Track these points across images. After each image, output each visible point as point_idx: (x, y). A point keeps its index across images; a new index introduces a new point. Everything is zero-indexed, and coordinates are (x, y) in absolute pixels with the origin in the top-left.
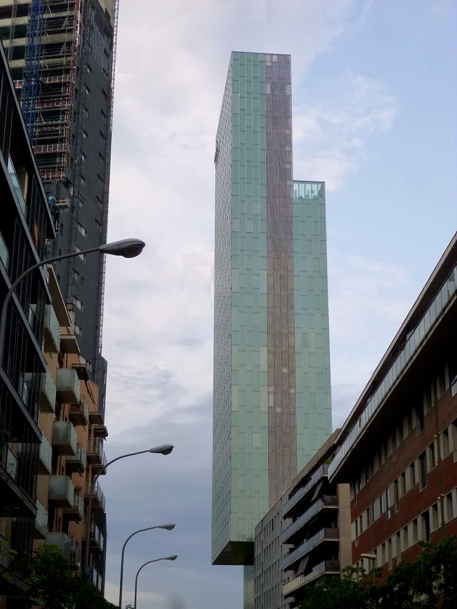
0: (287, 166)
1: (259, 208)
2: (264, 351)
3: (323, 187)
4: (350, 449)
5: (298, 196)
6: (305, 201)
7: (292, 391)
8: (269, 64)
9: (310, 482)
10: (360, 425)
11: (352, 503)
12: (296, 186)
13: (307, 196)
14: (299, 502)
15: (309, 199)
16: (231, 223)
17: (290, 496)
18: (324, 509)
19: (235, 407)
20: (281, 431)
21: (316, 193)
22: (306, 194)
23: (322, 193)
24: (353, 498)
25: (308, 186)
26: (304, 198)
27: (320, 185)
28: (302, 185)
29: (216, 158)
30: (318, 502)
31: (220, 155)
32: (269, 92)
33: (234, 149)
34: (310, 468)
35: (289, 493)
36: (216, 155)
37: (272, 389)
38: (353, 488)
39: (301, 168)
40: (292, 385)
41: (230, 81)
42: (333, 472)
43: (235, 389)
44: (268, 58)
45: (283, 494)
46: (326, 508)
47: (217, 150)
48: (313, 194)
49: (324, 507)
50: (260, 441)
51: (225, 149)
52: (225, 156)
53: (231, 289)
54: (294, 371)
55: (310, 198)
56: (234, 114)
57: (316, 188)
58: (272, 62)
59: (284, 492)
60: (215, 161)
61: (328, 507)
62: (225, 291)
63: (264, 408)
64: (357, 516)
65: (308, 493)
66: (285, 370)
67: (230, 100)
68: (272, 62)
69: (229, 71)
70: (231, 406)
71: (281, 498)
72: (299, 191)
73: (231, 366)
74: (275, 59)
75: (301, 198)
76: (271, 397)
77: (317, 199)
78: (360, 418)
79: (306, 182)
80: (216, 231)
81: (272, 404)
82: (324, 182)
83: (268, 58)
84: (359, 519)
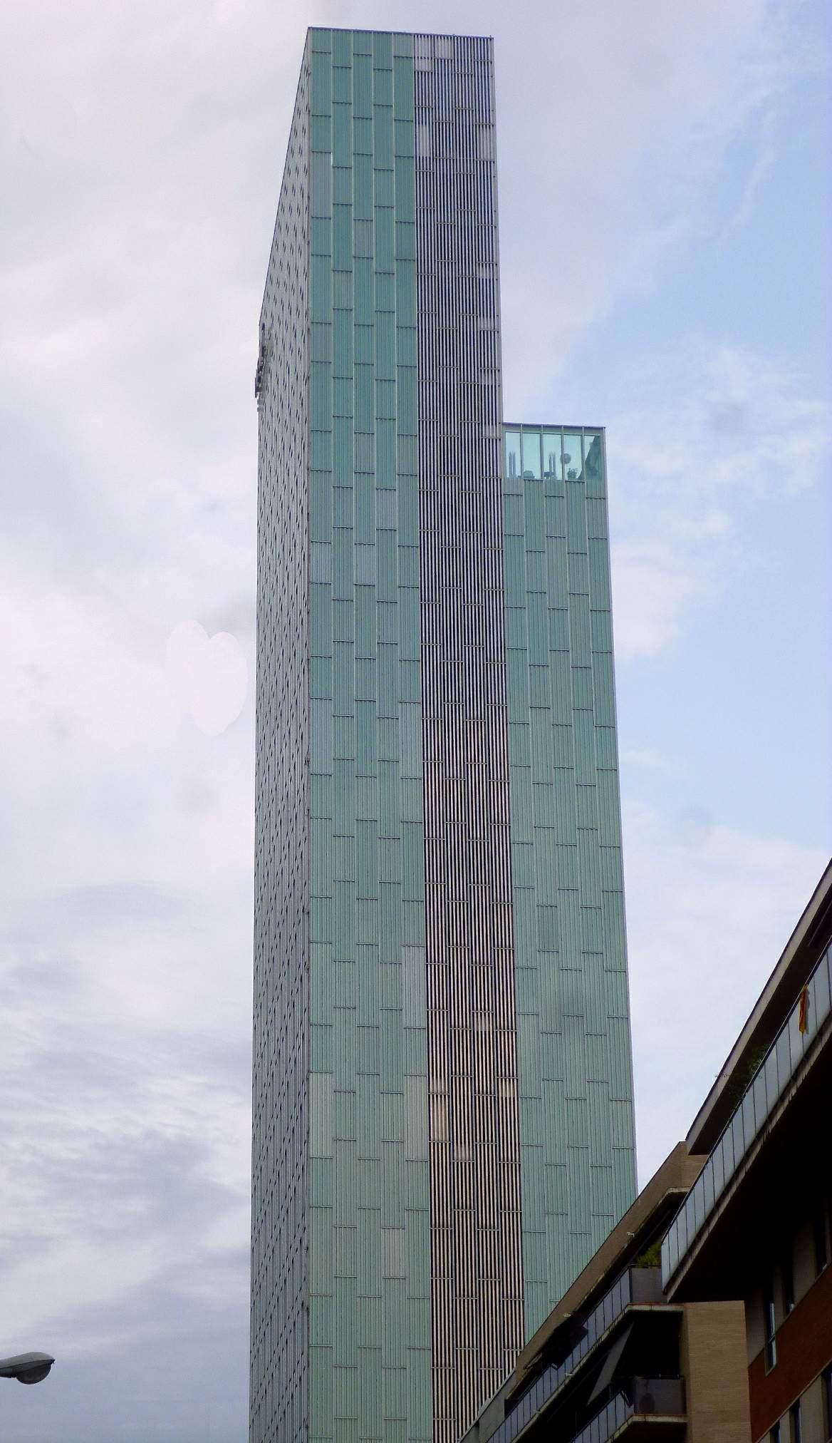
0: (487, 380)
1: (396, 509)
2: (414, 966)
3: (598, 446)
4: (758, 1136)
5: (518, 473)
6: (544, 489)
7: (507, 1091)
8: (424, 66)
9: (584, 1342)
10: (803, 1024)
11: (756, 1369)
12: (511, 440)
13: (547, 474)
14: (543, 1417)
15: (556, 483)
16: (308, 557)
17: (510, 1405)
18: (635, 1424)
19: (319, 1144)
20: (471, 1207)
21: (576, 465)
22: (546, 469)
23: (595, 462)
24: (759, 1345)
25: (552, 441)
26: (537, 476)
27: (589, 440)
28: (532, 439)
29: (259, 380)
30: (611, 1406)
31: (273, 365)
32: (424, 149)
33: (317, 325)
34: (580, 1298)
35: (507, 1394)
36: (260, 369)
37: (440, 1086)
38: (756, 1314)
39: (529, 386)
40: (505, 1072)
41: (304, 120)
42: (683, 1250)
43: (321, 1087)
44: (423, 48)
45: (482, 1409)
46: (646, 1423)
47: (263, 350)
48: (567, 468)
49: (637, 1419)
50: (403, 1253)
51: (289, 337)
52: (292, 364)
53: (307, 762)
54: (513, 1030)
55: (559, 477)
56: (317, 218)
57: (576, 449)
58: (435, 60)
59: (486, 1405)
60: (257, 389)
61: (651, 1419)
62: (286, 892)
63: (417, 1146)
64: (778, 1413)
65: (574, 1381)
66: (483, 1025)
67: (302, 180)
68: (435, 60)
69: (300, 90)
70: (307, 1142)
71: (477, 1425)
72: (523, 458)
73: (307, 1010)
74: (444, 50)
75: (528, 479)
76: (440, 1113)
77: (581, 481)
78: (806, 993)
79: (546, 427)
80: (259, 603)
81: (440, 1133)
82: (601, 429)
83: (423, 48)
84: (785, 1421)
